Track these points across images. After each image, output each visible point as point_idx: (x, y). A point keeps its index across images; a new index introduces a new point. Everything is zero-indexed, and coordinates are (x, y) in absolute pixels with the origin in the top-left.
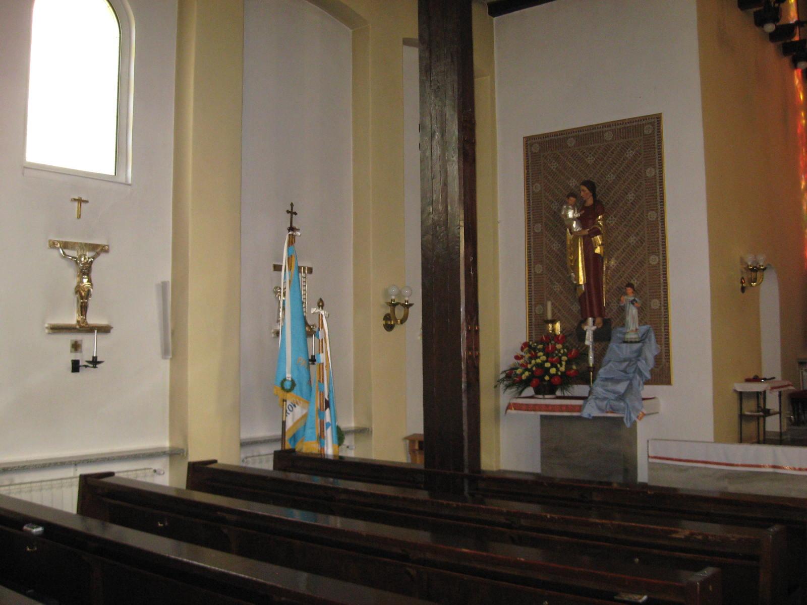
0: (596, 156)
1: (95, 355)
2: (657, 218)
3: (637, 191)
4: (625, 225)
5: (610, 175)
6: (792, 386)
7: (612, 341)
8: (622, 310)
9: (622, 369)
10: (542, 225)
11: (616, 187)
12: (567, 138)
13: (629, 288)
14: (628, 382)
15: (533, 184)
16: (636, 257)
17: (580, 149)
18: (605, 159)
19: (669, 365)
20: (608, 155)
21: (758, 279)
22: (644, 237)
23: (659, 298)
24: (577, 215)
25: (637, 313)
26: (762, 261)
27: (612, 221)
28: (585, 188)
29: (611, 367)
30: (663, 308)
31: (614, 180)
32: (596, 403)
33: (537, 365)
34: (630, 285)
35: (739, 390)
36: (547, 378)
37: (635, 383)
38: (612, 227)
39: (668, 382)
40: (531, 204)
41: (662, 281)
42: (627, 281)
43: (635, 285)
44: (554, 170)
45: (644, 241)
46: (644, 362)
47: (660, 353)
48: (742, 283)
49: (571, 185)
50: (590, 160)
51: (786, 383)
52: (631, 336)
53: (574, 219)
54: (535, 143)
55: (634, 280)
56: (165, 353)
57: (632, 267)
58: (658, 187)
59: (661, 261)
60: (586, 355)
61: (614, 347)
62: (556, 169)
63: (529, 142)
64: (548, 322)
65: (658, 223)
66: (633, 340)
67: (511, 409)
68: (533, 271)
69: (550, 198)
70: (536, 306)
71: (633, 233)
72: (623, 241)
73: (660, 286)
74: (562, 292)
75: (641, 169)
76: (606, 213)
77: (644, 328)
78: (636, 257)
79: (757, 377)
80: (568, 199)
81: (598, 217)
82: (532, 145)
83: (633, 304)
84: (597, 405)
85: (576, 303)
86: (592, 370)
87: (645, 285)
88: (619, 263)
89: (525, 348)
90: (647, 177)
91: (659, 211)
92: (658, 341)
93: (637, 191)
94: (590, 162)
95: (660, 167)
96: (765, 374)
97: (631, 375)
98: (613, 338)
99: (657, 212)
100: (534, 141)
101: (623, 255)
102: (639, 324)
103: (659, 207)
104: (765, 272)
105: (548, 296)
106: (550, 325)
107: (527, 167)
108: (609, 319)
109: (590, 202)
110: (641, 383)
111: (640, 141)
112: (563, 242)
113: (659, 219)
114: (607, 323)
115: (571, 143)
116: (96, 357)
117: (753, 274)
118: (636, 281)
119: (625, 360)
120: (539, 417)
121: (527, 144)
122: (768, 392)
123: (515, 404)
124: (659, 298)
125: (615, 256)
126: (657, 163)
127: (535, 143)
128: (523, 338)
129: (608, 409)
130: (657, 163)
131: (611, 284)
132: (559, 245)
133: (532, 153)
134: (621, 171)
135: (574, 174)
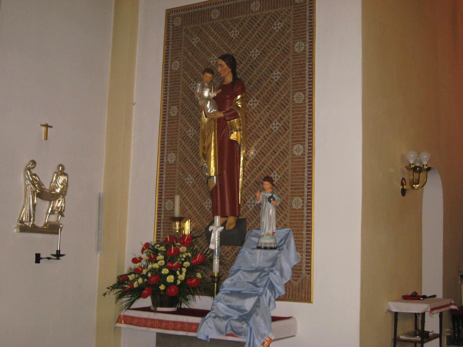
0: (241, 29)
1: (58, 250)
2: (304, 100)
3: (283, 69)
4: (268, 108)
5: (255, 51)
6: (455, 304)
7: (244, 246)
8: (259, 208)
9: (251, 281)
10: (178, 107)
11: (260, 64)
12: (211, 9)
13: (267, 182)
14: (256, 298)
15: (172, 62)
16: (278, 146)
17: (224, 22)
18: (250, 32)
19: (310, 277)
20: (254, 27)
21: (420, 181)
22: (289, 122)
23: (302, 196)
24: (214, 95)
25: (274, 213)
26: (425, 159)
27: (253, 103)
28: (223, 63)
29: (239, 278)
30: (305, 208)
31: (259, 56)
32: (214, 322)
33: (153, 270)
34: (268, 179)
35: (394, 310)
36: (162, 287)
37: (265, 300)
38: (253, 111)
39: (307, 298)
40: (169, 84)
41: (306, 175)
42: (267, 175)
43: (276, 179)
44: (195, 45)
45: (288, 127)
46: (278, 273)
47: (300, 262)
48: (402, 184)
49: (211, 62)
50: (234, 34)
51: (448, 302)
52: (267, 241)
53: (208, 99)
54: (177, 16)
55: (275, 174)
56: (98, 249)
57: (273, 157)
58: (307, 64)
59: (307, 151)
60: (211, 260)
61: (247, 253)
62: (197, 44)
63: (171, 15)
64: (175, 219)
65: (305, 107)
66: (268, 246)
67: (121, 323)
68: (165, 160)
69: (189, 77)
70: (165, 201)
71: (276, 117)
72: (265, 127)
73: (303, 182)
74: (195, 185)
75: (289, 43)
76: (247, 93)
77: (284, 232)
78: (278, 146)
79: (416, 293)
80: (203, 75)
81: (237, 96)
82: (174, 18)
83: (270, 202)
84: (216, 326)
85: (209, 199)
86: (216, 280)
87: (287, 180)
88: (259, 154)
89: (146, 249)
90: (296, 52)
91: (307, 92)
92: (298, 249)
93: (283, 69)
94: (234, 36)
95: (311, 40)
96: (426, 291)
97: (261, 290)
98: (247, 242)
99: (304, 94)
100: (176, 14)
101: (264, 144)
102: (277, 226)
103: (307, 87)
104: (429, 172)
105: (180, 190)
106: (177, 224)
107: (167, 43)
108: (244, 220)
109: (229, 79)
110: (273, 299)
111: (290, 11)
112: (197, 126)
113: (306, 102)
114: (241, 223)
115: (215, 14)
116: (59, 251)
117: (416, 175)
118: (276, 175)
119: (256, 270)
120: (155, 334)
121: (169, 17)
122: (427, 315)
123: (125, 316)
124: (302, 196)
125: (255, 144)
126: (307, 36)
127: (177, 16)
128: (151, 238)
129: (229, 331)
130: (307, 36)
131: (248, 178)
132: (195, 131)
133: (173, 28)
134: (267, 46)
135: (216, 50)
